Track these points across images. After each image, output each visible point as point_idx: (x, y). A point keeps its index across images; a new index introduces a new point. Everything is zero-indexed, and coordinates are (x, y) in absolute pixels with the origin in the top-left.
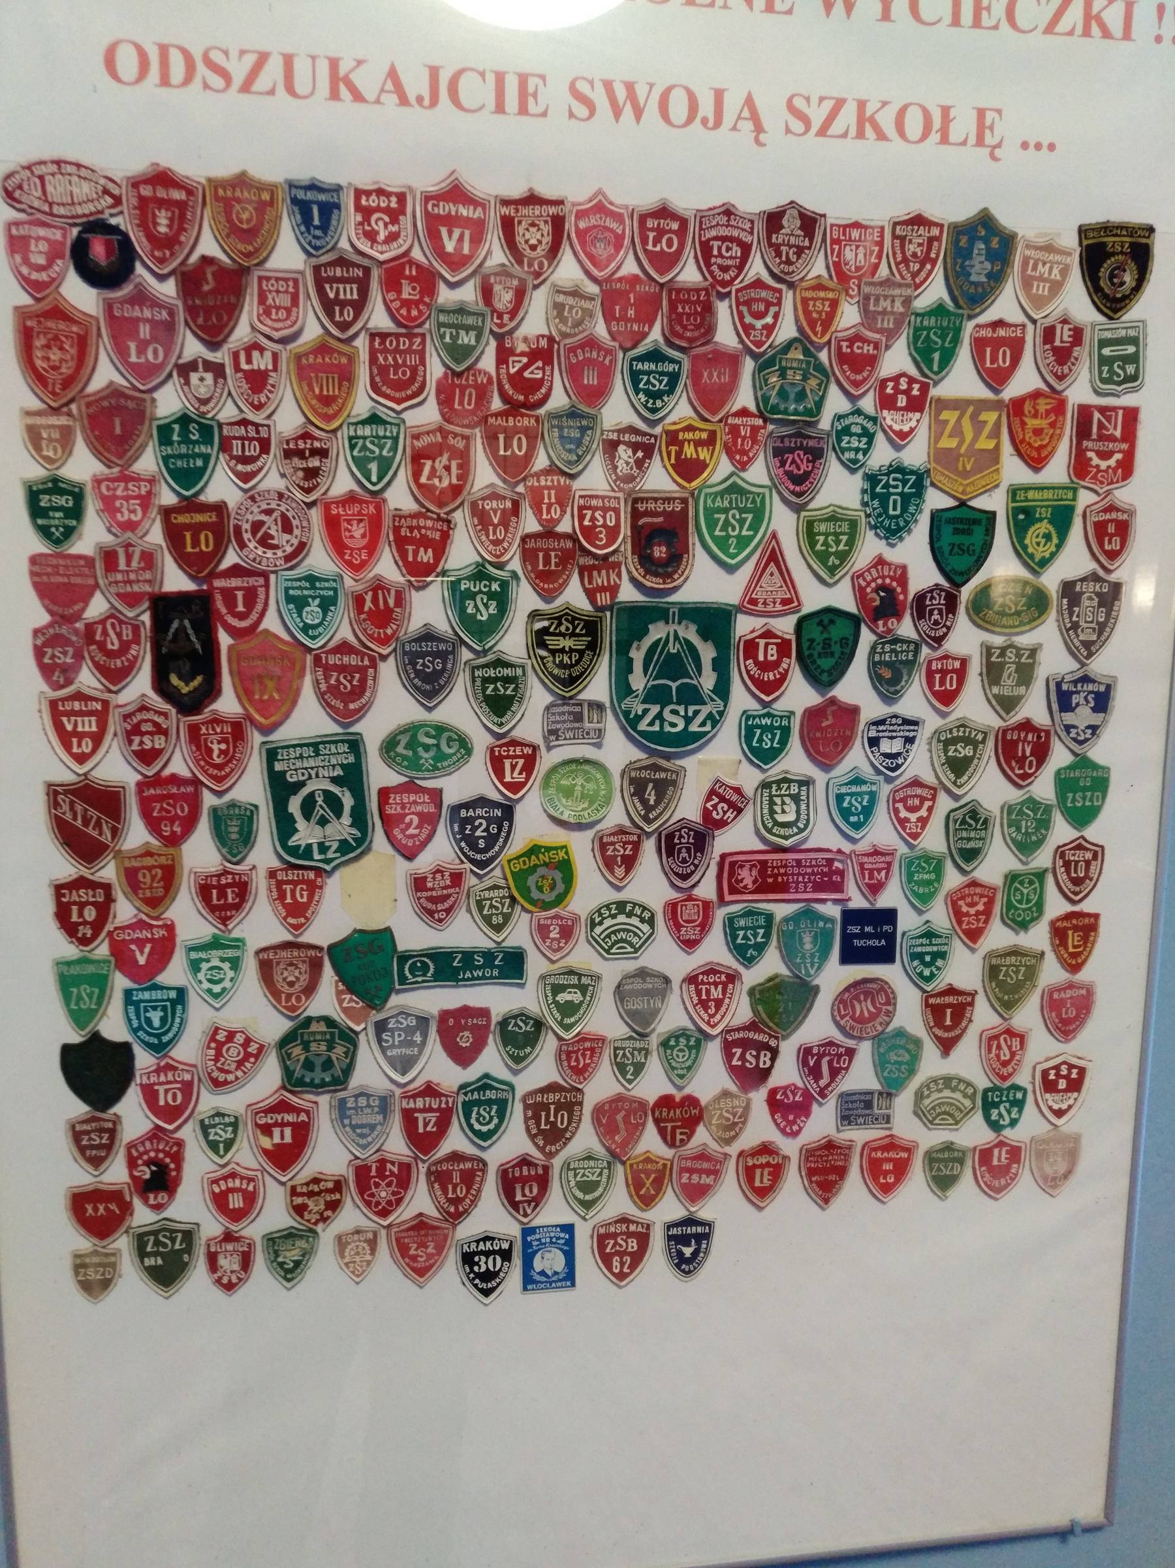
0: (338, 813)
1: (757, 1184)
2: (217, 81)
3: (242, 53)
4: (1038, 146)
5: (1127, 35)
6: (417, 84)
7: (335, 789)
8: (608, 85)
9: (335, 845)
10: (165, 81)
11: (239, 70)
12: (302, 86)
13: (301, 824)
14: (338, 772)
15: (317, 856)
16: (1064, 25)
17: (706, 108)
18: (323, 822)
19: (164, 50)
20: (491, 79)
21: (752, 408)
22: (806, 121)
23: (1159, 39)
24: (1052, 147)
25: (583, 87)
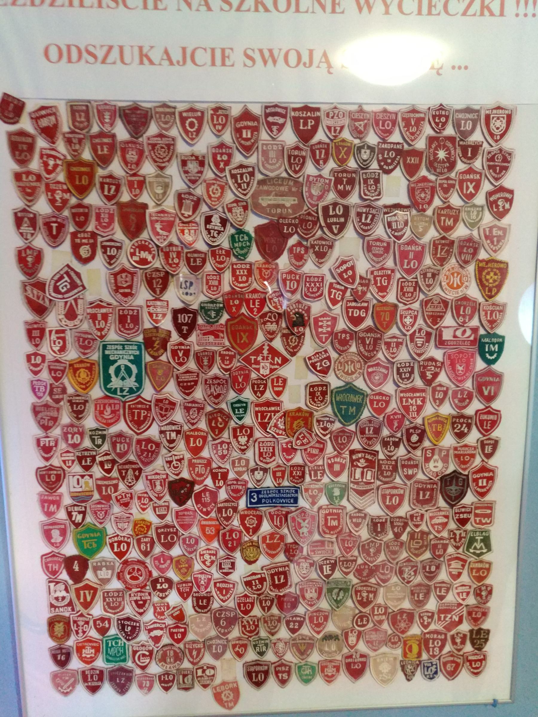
0: (130, 376)
1: (118, 451)
2: (91, 59)
3: (102, 46)
4: (460, 68)
5: (502, 14)
6: (176, 56)
7: (130, 365)
8: (261, 51)
9: (127, 389)
10: (70, 61)
11: (100, 54)
12: (127, 59)
13: (114, 378)
14: (132, 358)
15: (119, 393)
16: (471, 11)
17: (305, 58)
18: (123, 379)
19: (69, 47)
20: (209, 51)
21: (405, 201)
22: (95, 57)
23: (517, 15)
24: (466, 68)
25: (249, 52)
